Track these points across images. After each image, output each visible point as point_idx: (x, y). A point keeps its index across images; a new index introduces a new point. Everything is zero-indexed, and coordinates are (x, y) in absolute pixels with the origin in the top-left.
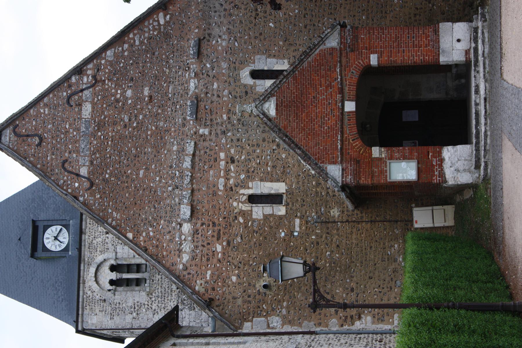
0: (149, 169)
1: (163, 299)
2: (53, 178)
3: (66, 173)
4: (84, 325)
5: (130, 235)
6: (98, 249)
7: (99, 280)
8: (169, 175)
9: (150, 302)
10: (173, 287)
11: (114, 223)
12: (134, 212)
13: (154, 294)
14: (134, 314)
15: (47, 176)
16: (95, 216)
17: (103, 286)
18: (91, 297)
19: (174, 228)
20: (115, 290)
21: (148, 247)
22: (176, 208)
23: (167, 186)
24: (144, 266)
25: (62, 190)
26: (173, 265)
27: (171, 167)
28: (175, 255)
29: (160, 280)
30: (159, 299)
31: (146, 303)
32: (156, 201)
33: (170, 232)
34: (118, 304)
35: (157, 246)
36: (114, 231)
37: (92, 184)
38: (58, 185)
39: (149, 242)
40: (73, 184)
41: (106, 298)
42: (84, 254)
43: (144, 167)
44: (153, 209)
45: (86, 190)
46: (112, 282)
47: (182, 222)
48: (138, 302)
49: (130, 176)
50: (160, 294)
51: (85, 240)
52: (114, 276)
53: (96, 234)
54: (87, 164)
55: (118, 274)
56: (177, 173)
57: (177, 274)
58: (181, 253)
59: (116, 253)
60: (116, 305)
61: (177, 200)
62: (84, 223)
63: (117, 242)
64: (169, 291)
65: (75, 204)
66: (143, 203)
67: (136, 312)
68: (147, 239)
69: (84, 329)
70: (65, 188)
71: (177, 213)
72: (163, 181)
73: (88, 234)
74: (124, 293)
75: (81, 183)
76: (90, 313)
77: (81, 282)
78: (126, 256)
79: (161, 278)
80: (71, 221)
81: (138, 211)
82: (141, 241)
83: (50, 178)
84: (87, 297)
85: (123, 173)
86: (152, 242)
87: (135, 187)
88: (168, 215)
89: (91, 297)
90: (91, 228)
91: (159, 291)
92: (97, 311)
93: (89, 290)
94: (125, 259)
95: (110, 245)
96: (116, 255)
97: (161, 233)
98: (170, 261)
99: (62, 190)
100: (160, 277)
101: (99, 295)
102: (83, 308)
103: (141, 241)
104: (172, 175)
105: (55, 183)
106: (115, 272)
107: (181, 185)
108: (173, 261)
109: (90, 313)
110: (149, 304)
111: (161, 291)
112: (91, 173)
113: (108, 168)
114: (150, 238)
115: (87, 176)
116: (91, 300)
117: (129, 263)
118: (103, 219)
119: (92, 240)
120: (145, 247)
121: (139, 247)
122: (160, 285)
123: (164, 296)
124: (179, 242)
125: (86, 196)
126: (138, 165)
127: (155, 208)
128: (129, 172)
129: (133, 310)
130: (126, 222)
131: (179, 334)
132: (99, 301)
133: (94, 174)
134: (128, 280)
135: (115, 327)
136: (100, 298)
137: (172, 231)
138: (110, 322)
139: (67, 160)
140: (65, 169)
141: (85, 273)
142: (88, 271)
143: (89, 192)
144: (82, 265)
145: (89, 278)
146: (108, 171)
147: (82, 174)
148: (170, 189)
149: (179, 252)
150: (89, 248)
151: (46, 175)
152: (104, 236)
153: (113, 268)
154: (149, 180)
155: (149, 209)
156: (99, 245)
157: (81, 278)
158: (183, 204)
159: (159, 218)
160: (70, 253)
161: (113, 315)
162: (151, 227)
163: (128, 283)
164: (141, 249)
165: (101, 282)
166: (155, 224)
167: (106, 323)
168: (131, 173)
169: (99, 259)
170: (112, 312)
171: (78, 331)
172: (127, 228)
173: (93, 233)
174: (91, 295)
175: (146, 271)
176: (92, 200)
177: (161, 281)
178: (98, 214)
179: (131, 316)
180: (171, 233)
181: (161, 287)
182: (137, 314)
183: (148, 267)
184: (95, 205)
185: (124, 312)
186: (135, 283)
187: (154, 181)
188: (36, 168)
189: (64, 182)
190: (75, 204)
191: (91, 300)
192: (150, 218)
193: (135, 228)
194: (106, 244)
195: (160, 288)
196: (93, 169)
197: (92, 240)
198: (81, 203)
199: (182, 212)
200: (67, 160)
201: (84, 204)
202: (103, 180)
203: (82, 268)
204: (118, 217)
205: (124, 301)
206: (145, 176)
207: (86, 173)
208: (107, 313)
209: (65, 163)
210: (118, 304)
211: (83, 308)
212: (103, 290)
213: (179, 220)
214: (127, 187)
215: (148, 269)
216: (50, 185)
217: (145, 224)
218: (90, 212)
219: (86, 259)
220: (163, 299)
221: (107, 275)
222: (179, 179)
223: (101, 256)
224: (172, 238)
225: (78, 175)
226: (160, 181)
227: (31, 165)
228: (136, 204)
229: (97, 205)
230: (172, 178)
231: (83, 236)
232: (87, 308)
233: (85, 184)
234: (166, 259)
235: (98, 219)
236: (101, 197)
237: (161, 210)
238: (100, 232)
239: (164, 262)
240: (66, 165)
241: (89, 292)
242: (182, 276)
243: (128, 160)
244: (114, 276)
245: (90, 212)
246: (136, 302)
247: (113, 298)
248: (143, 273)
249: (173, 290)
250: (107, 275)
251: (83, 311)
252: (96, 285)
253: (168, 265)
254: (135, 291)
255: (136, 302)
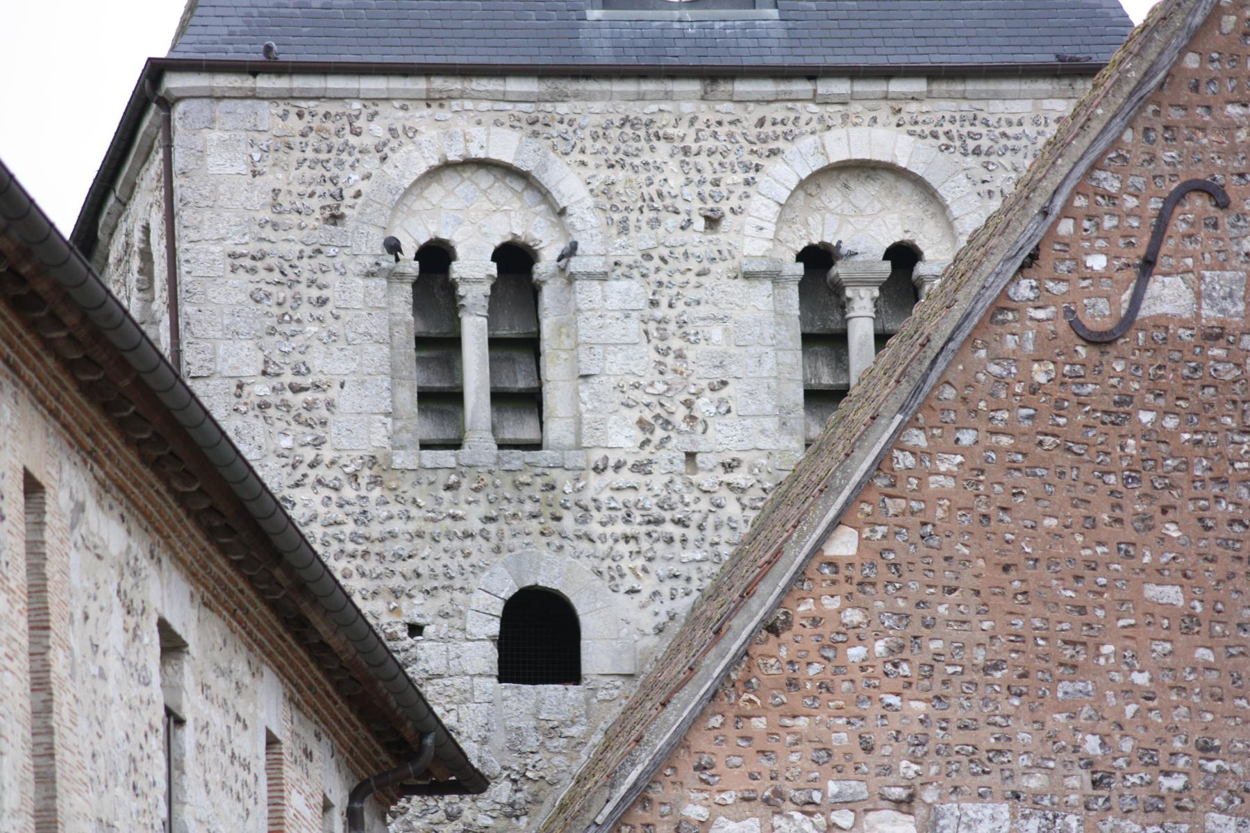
0: (1188, 631)
1: (350, 547)
2: (1128, 136)
3: (1155, 204)
4: (195, 104)
5: (844, 545)
6: (619, 175)
7: (451, 181)
8: (1161, 740)
9: (329, 475)
10: (419, 599)
11: (904, 460)
12: (966, 561)
13: (377, 492)
14: (261, 389)
15: (1142, 109)
16: (941, 364)
17: (418, 205)
18: (353, 140)
19: (888, 770)
20: (394, 276)
21: (786, 636)
22: (994, 779)
23: (1104, 727)
24: (527, 432)
25: (1066, 191)
26: (700, 768)
27: (1206, 748)
28: (752, 777)
29: (459, 527)
30: (350, 527)
31: (327, 454)
32: (1024, 676)
33: (868, 749)
34: (315, 293)
35: (792, 684)
36: (865, 466)
37: (1100, 341)
38: (1094, 166)
39: (812, 645)
40: (1101, 243)
41: (350, 224)
42: (590, 97)
43: (1199, 608)
44: (980, 656)
45: (1069, 312)
46: (436, 256)
47: (921, 811)
48: (330, 405)
49: (1151, 537)
50: (375, 530)
51: (668, 96)
52: (474, 268)
53: (703, 160)
54: (1206, 311)
55: (486, 289)
56: (1177, 782)
57: (657, 794)
58: (762, 809)
59: (603, 277)
60: (312, 283)
61: (1035, 782)
62: (767, 87)
63: (662, 276)
64: (397, 582)
65: (997, 258)
66: (1010, 605)
67: (274, 399)
68: (826, 630)
69: (167, 104)
70: (1080, 202)
71: (970, 784)
72: (1131, 709)
73: (705, 112)
74: (378, 326)
75: (1106, 286)
76: (263, 139)
77: (438, 83)
78: (587, 329)
79: (468, 535)
80: (774, 13)
81: (968, 580)
82: (817, 599)
83: (1130, 125)
84: (352, 119)
85: (1166, 498)
86: (814, 656)
87: (1092, 565)
88: (956, 738)
89: (353, 140)
90: (737, 130)
91: (397, 526)
92: (274, 178)
93: (392, 131)
94: (568, 327)
95: (644, 239)
96: (590, 276)
97: (859, 701)
98: (720, 756)
99: (1066, 191)
100: (475, 525)
101: (364, 186)
102: (290, 97)
103: (817, 599)
104: (1162, 757)
105: (1104, 153)
106: (493, 269)
107: (1115, 800)
108: (721, 767)
109: (263, 139)
110: (321, 471)
111: (393, 535)
112: (1159, 335)
113: (1187, 419)
114: (833, 645)
115: (1144, 312)
116: (337, 142)
117: (546, 346)
118: (926, 406)
119: (668, 138)
120: (788, 624)
121: (787, 591)
122: (429, 528)
123: (366, 553)
124: (817, 796)
125: (1040, 314)
126: (1210, 575)
127: (986, 670)
128: (1173, 531)
129: (288, 378)
130: (910, 520)
131: (367, 818)
132: (329, 187)
133: (1153, 347)
134: (453, 343)
135: (184, 278)
136: (348, 193)
137: (872, 759)
138: (217, 249)
139: (1222, 202)
140: (1177, 198)
141: (485, 105)
142: (498, 123)
143: (1063, 326)
144: (530, 86)
145: (461, 125)
146: (1171, 423)
147: (1156, 286)
148: (1092, 745)
149: (767, 801)
150: (625, 121)
151: (1144, 102)
152: (697, 204)
153: (514, 260)
154: (1129, 634)
155: (984, 638)
156: (643, 176)
157: (455, 85)
158: (1013, 815)
159: (938, 689)
160: (594, 14)
161: (253, 270)
162: (891, 651)
163: (439, 345)
164: (779, 603)
165: (435, 192)
166: (905, 668)
167: (207, 232)
168: (1163, 539)
169: (568, 183)
170: (272, 261)
171: (155, 70)
172: (882, 530)
173: (710, 143)
174: (366, 140)
175: (501, 447)
176: (1020, 346)
177: (450, 535)
178: (950, 377)
179: (251, 370)
180: (861, 756)
181: (420, 535)
182: (263, 406)
183: (529, 456)
184: (996, 359)
185: (272, 332)
186: (437, 383)
187: (1127, 662)
188: (1182, 52)
189: (1111, 197)
190: (997, 258)
191: (337, 142)
192: (936, 645)
193: (882, 568)
194: (648, 215)
195: (412, 527)
196: (1180, 346)
197: (668, 138)
198: (1004, 292)
199: (971, 809)
200: (1222, 202)
201: (1001, 306)
202: (1126, 400)
203: (515, 86)
204: (934, 482)
205: (335, 326)
206: (1151, 613)
207: (1160, 309)
208: (268, 232)
209: (1211, 195)
210: (315, 293)
211: (290, 97)
212: (395, 208)
213: (930, 795)
214: (1091, 522)
215: (517, 458)
216: (1096, 126)
217: (904, 617)
218: (960, 337)
219: (562, 108)
220: (350, 547)
221: (475, 227)
222: (1143, 794)
223: (583, 192)
224: (838, 759)
225: (1148, 266)
226: (1128, 692)
227: (1198, 19)
228: (1006, 568)
229: (995, 369)
230: (1147, 757)
231: (695, 86)
232: (293, 117)
233: (1102, 305)
234: (731, 732)
235: (925, 378)
236: (1034, 389)
237: (976, 701)
238: (716, 183)
239: (716, 721)
240: (1199, 203)
241: (378, 129)
242: (648, 817)
243: (1232, 522)
244: (474, 268)
245: (960, 337)
246: (333, 393)
247: (352, 267)
248: (494, 430)
249: (404, 603)
250: (475, 227)
251: (275, 98)
252: (423, 168)
253: (701, 742)
254: (392, 390)
255: (333, 393)
